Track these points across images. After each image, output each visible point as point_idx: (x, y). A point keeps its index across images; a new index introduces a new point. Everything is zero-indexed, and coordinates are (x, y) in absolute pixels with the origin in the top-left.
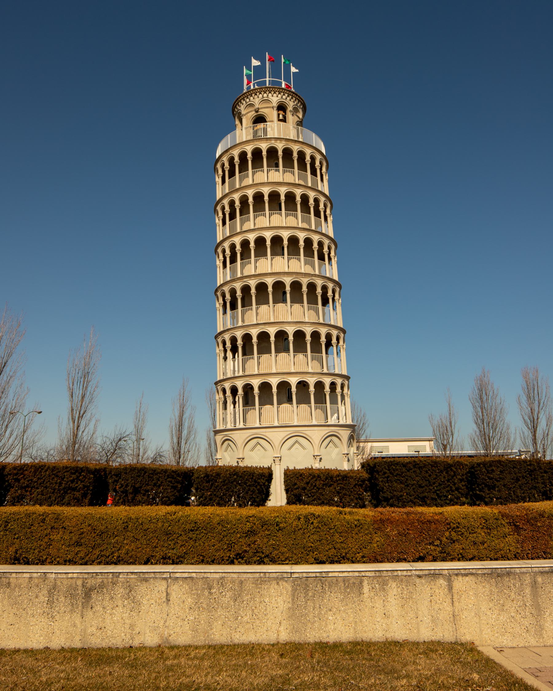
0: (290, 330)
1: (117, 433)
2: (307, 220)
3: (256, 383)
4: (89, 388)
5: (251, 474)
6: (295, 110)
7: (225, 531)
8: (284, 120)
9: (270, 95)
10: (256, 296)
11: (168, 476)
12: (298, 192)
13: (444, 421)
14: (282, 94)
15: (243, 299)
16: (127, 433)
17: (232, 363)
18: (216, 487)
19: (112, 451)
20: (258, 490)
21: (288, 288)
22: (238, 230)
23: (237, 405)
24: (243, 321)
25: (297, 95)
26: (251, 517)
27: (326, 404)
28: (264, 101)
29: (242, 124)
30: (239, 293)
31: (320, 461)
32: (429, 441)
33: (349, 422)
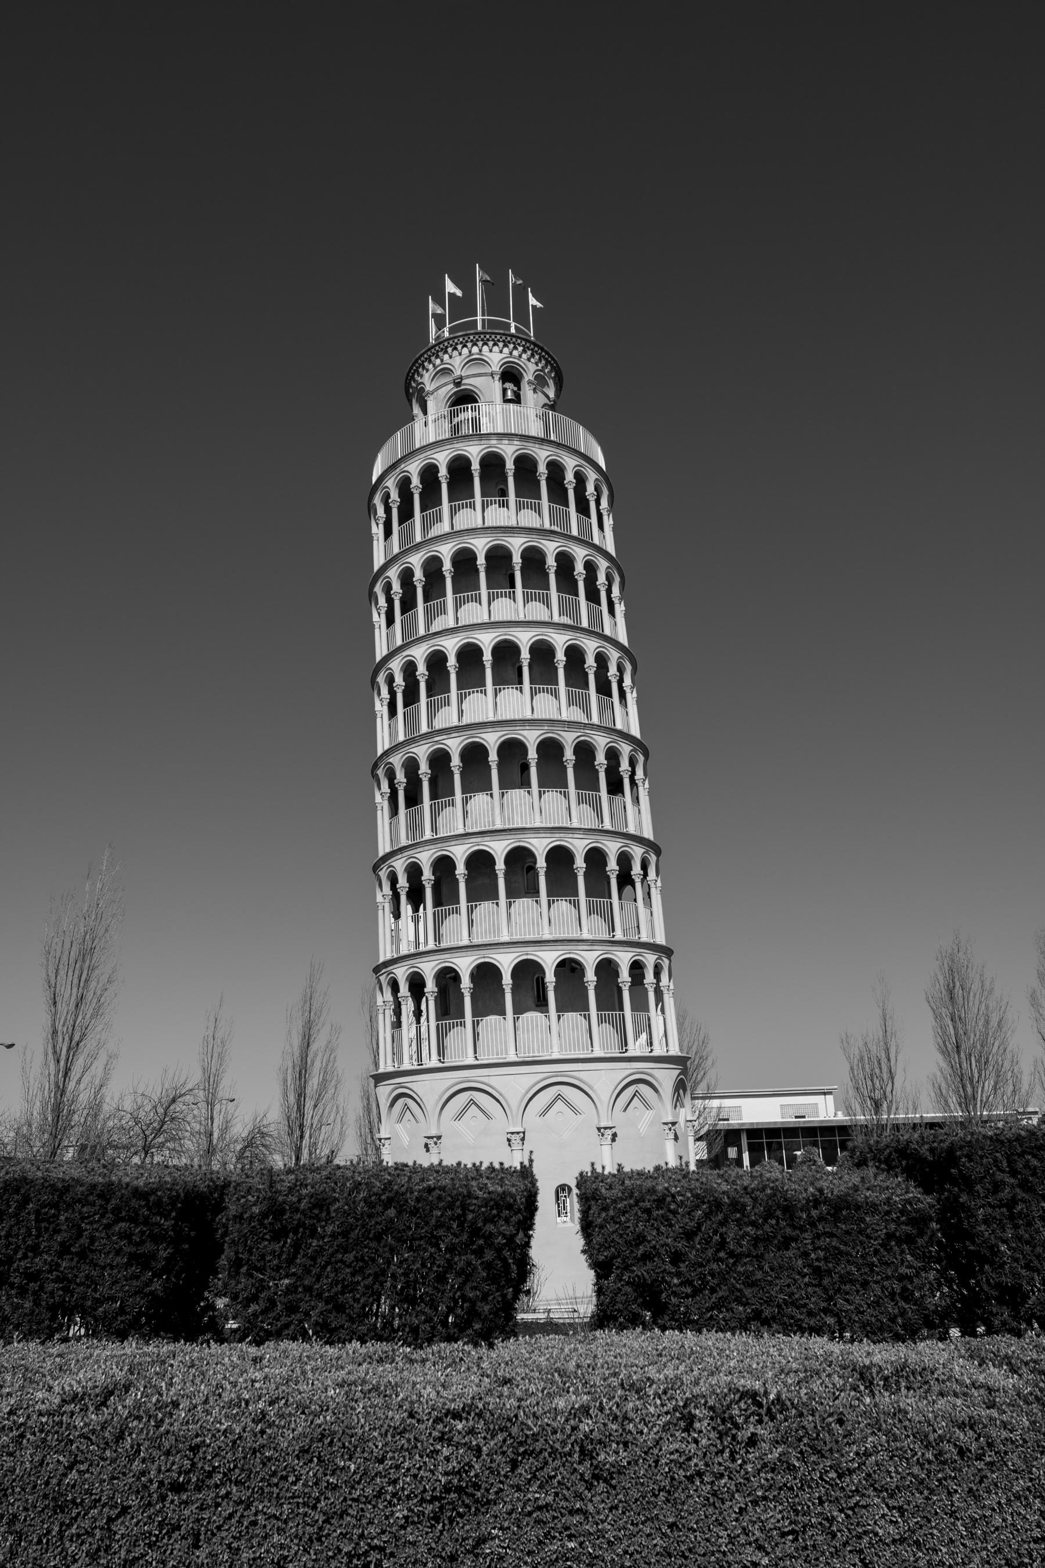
0: (540, 847)
1: (166, 1086)
2: (569, 609)
3: (465, 965)
4: (93, 984)
5: (455, 1199)
6: (540, 382)
7: (335, 1487)
8: (517, 400)
9: (485, 348)
10: (462, 774)
11: (117, 1210)
12: (551, 548)
13: (874, 1049)
14: (511, 346)
15: (433, 782)
16: (189, 1086)
17: (411, 925)
18: (313, 1259)
19: (155, 1125)
20: (488, 1266)
21: (532, 755)
22: (422, 632)
23: (423, 1019)
24: (434, 829)
25: (542, 349)
26: (456, 1416)
27: (610, 897)
28: (471, 361)
29: (425, 412)
30: (427, 875)
31: (613, 1140)
32: (825, 1094)
33: (674, 1050)
